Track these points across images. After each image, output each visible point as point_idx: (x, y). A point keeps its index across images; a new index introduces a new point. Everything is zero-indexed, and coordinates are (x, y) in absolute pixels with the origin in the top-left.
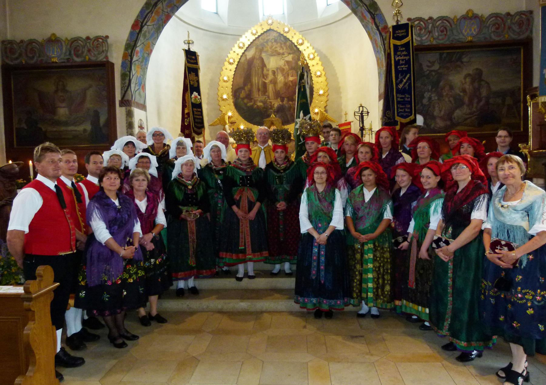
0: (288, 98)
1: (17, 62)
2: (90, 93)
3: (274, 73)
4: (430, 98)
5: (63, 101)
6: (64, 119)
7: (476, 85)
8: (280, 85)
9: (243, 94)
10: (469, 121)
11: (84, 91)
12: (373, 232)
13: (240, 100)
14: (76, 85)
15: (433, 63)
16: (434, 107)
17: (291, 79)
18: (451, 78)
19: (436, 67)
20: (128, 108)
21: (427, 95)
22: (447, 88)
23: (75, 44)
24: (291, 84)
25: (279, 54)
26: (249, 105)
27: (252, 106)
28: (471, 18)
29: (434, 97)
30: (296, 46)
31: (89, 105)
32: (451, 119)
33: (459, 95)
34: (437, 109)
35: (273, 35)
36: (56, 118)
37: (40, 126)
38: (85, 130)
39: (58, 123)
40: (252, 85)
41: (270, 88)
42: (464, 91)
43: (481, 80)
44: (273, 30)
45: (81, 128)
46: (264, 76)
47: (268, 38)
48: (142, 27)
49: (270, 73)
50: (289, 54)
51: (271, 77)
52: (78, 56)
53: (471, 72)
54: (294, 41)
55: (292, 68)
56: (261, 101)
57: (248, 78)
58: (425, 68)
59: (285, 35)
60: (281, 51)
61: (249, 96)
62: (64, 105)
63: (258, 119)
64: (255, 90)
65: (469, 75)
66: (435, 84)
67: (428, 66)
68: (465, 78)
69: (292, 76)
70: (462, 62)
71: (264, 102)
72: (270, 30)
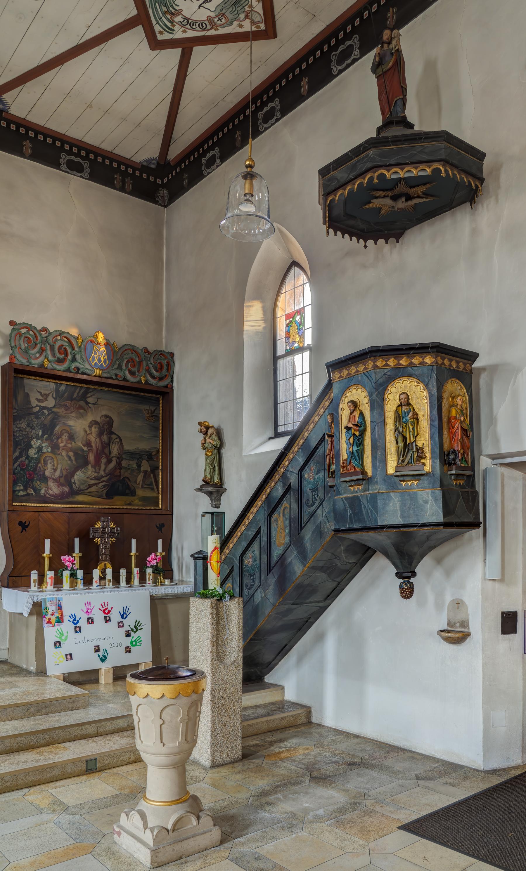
4: (40, 449)
7: (105, 438)
10: (94, 489)
15: (46, 397)
16: (46, 463)
18: (71, 423)
19: (50, 403)
21: (35, 443)
22: (65, 437)
29: (47, 448)
32: (69, 484)
33: (82, 450)
34: (49, 466)
42: (88, 444)
53: (98, 420)
58: (34, 402)
65: (96, 423)
66: (48, 430)
67: (38, 400)
68: (90, 427)
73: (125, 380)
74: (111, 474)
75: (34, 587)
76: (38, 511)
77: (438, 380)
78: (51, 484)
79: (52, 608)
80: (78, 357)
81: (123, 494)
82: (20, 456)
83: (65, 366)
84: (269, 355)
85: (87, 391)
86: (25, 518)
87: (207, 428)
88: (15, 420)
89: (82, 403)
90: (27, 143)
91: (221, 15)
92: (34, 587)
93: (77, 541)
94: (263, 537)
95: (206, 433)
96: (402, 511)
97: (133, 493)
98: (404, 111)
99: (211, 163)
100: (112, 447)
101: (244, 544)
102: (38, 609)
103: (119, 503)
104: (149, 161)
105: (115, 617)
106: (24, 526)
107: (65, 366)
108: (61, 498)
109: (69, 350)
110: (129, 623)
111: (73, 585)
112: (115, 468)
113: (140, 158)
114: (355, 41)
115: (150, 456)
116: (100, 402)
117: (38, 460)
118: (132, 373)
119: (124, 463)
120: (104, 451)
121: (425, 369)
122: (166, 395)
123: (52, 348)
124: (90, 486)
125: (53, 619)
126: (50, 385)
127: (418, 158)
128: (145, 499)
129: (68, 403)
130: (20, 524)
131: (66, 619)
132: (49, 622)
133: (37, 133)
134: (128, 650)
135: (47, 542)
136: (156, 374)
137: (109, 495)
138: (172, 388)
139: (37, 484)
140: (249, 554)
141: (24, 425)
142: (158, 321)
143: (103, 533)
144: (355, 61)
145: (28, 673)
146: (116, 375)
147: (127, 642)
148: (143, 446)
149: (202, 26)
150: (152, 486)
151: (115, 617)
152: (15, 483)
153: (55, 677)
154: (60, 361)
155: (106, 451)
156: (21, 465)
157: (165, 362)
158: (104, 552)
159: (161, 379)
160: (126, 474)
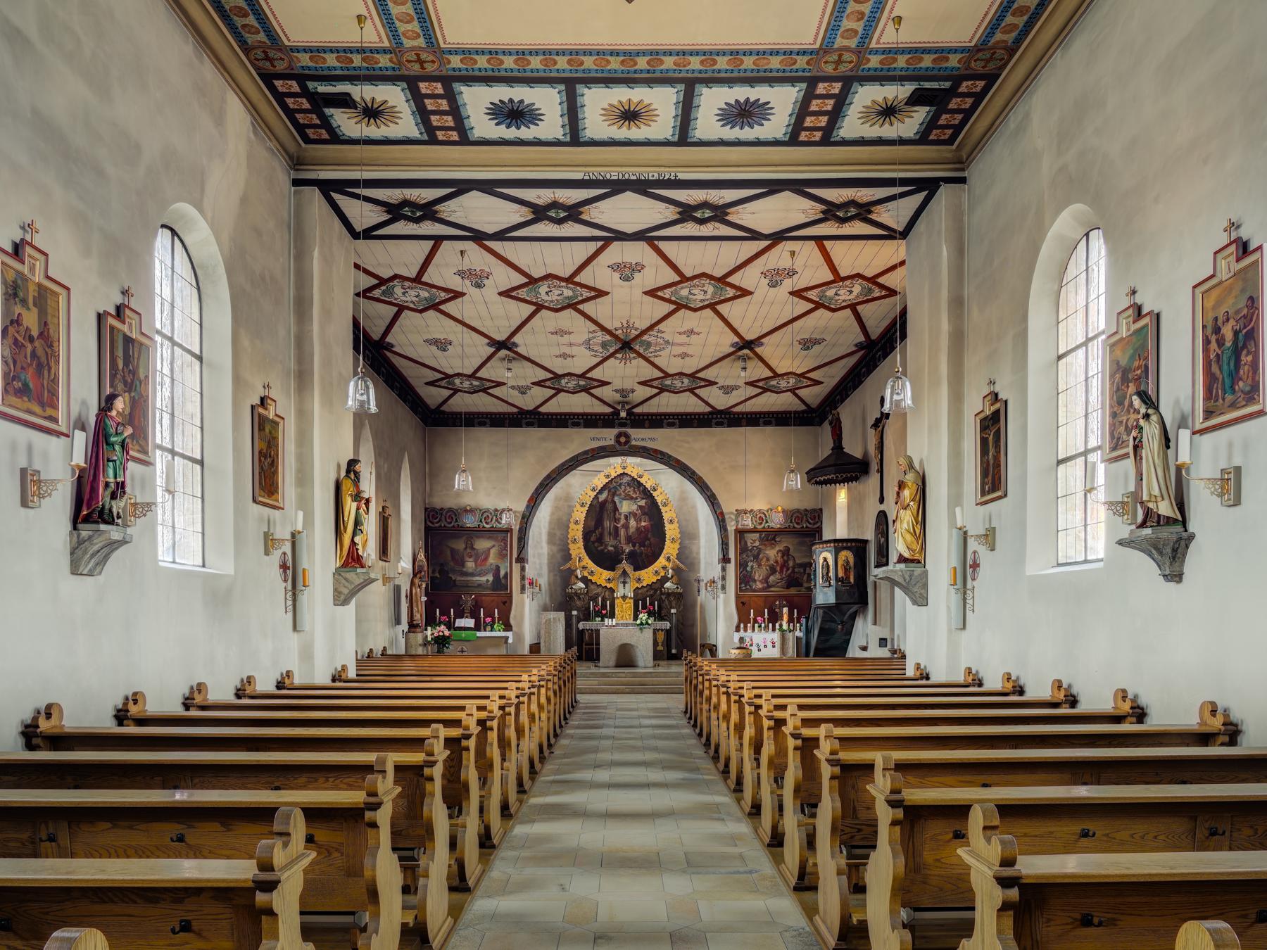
2: (492, 551)
3: (626, 517)
8: (632, 530)
11: (489, 549)
12: (797, 790)
14: (482, 544)
19: (757, 544)
23: (485, 514)
25: (632, 498)
29: (755, 566)
31: (492, 560)
35: (626, 479)
39: (466, 574)
41: (622, 532)
45: (484, 579)
46: (617, 520)
51: (623, 521)
54: (648, 486)
55: (644, 514)
57: (599, 523)
61: (600, 540)
64: (606, 533)
66: (756, 557)
71: (615, 547)
72: (624, 474)
97: (801, 585)
103: (793, 591)
106: (743, 603)
108: (763, 590)
120: (784, 565)
137: (788, 587)
153: (513, 387)
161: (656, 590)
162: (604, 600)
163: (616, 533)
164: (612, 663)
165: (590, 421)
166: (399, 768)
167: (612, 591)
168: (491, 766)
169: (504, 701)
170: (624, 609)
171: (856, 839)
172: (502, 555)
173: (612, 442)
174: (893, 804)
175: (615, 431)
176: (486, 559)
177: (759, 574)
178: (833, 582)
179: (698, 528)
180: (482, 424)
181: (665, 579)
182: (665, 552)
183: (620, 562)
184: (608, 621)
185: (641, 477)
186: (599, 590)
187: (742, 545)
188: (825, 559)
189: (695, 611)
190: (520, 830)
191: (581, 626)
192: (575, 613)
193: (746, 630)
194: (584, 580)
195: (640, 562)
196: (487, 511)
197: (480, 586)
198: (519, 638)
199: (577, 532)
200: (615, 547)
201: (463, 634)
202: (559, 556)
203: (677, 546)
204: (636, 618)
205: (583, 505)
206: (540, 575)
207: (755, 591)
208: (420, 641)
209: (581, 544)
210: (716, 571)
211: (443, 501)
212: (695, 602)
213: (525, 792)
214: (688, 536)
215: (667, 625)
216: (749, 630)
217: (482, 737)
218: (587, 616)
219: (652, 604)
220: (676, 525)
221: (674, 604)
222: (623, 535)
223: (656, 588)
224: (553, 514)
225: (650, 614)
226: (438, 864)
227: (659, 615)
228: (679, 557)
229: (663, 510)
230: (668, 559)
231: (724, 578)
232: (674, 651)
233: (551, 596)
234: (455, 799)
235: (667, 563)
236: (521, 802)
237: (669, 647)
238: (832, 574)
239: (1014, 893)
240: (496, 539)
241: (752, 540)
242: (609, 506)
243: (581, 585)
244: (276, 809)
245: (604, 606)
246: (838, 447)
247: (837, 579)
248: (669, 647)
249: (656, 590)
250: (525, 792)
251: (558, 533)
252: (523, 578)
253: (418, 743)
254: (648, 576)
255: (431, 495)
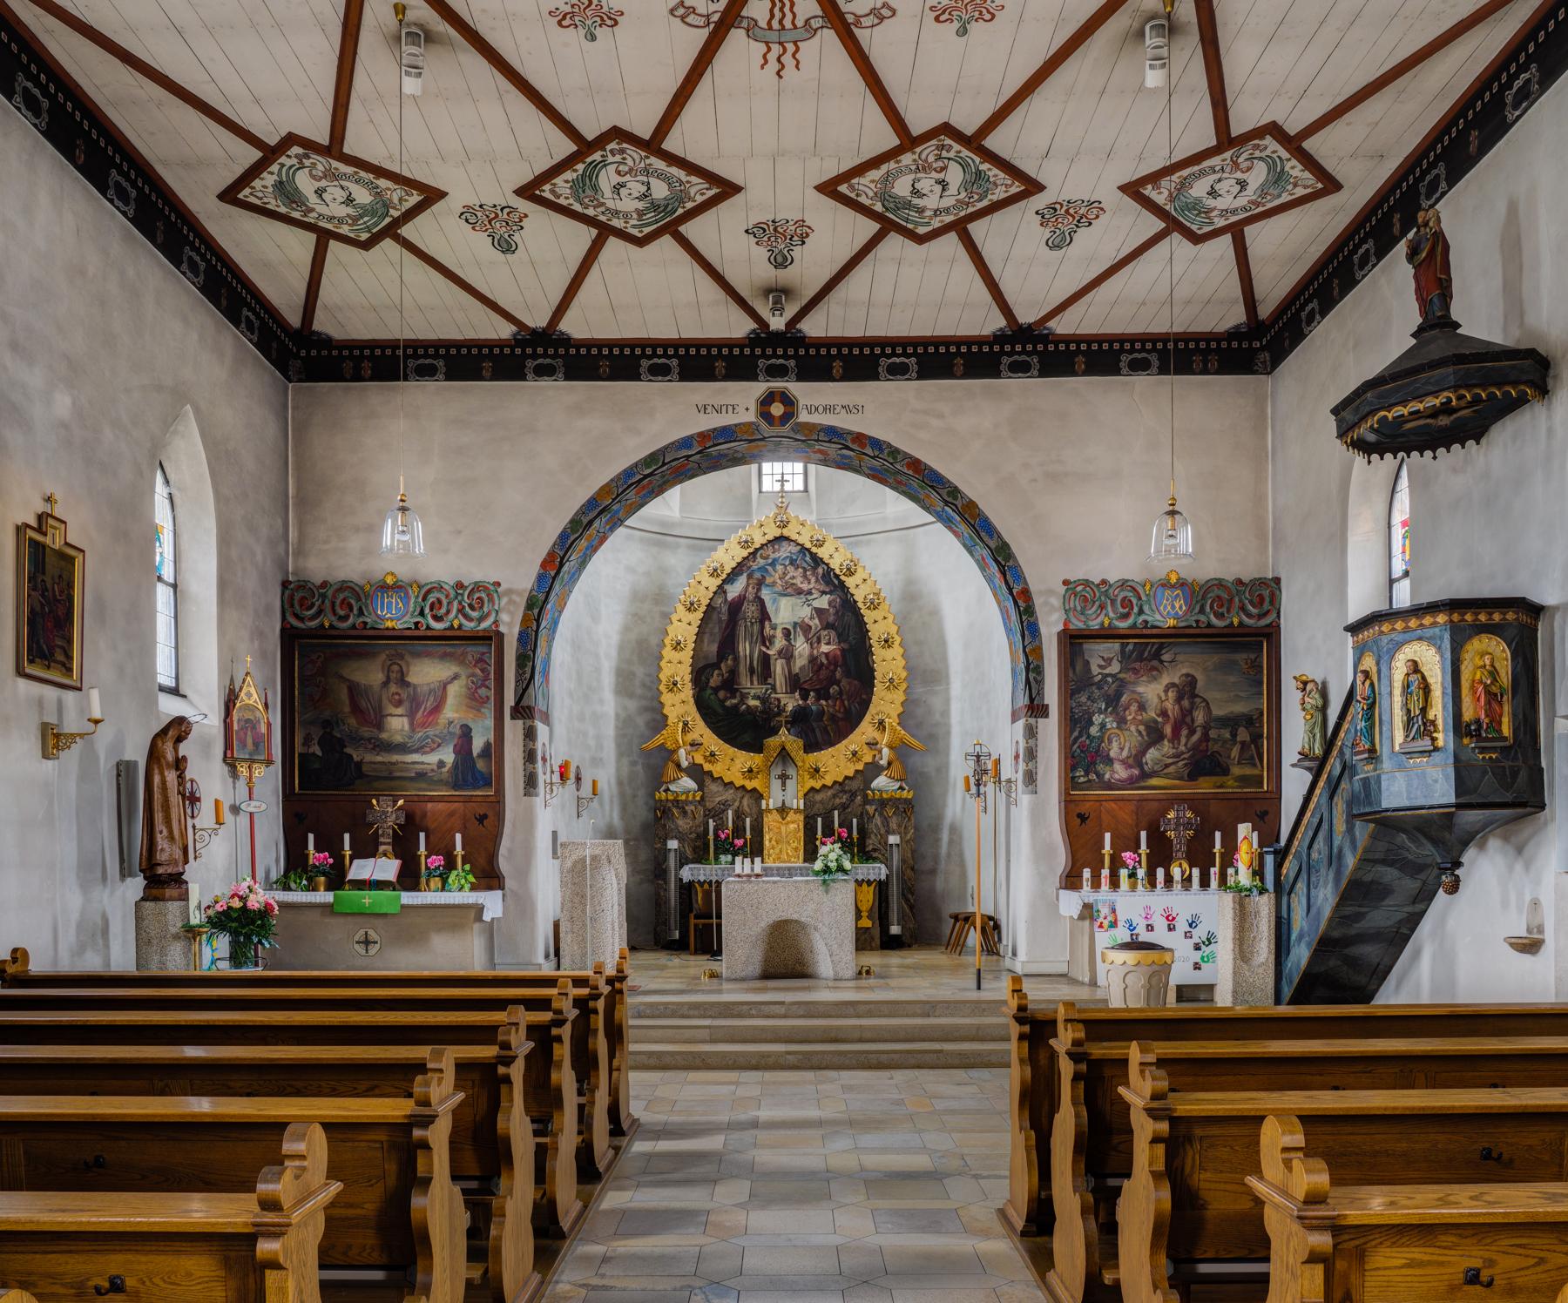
0: (817, 691)
1: (313, 624)
2: (454, 690)
4: (1103, 725)
5: (399, 704)
6: (398, 739)
7: (1186, 703)
8: (800, 662)
9: (715, 680)
10: (1171, 769)
13: (709, 691)
14: (427, 673)
15: (1109, 661)
16: (1110, 741)
17: (825, 648)
18: (1140, 689)
19: (1115, 668)
20: (529, 722)
21: (1097, 719)
22: (1134, 708)
23: (430, 596)
24: (824, 661)
25: (799, 592)
26: (728, 703)
27: (736, 707)
28: (1173, 587)
29: (1111, 723)
30: (837, 576)
31: (453, 711)
32: (1140, 765)
33: (1156, 722)
34: (1115, 745)
36: (384, 736)
37: (348, 750)
38: (441, 764)
40: (736, 659)
41: (779, 667)
42: (1164, 713)
43: (1193, 696)
44: (787, 539)
45: (432, 759)
46: (766, 641)
47: (777, 555)
48: (561, 565)
49: (779, 633)
50: (823, 593)
51: (780, 643)
52: (437, 618)
53: (1176, 681)
54: (835, 564)
55: (827, 626)
56: (756, 697)
57: (728, 645)
58: (1095, 670)
59: (814, 550)
60: (805, 587)
61: (730, 684)
62: (399, 711)
63: (747, 738)
64: (743, 670)
65: (1173, 685)
66: (1113, 701)
67: (1100, 667)
68: (1166, 691)
69: (828, 644)
70: (1162, 662)
71: (764, 700)
73: (1209, 625)
74: (1195, 748)
75: (1086, 887)
76: (1100, 801)
77: (1453, 641)
78: (1117, 766)
79: (1105, 911)
80: (1146, 608)
81: (1211, 773)
82: (1080, 735)
83: (1130, 621)
84: (1383, 580)
85: (1161, 646)
86: (1084, 808)
87: (1305, 683)
88: (1072, 695)
89: (1155, 663)
90: (1081, 358)
91: (1263, 194)
92: (1086, 887)
93: (1143, 834)
94: (1325, 826)
95: (1304, 690)
96: (1409, 792)
97: (1225, 771)
98: (1446, 307)
99: (1310, 319)
100: (1195, 714)
101: (1311, 833)
102: (1088, 911)
103: (1205, 786)
104: (1237, 327)
105: (1182, 926)
106: (1083, 818)
107: (1130, 621)
108: (1131, 783)
109: (1134, 601)
110: (1200, 934)
111: (1133, 887)
112: (1200, 741)
113: (1224, 326)
114: (1441, 169)
115: (1251, 721)
116: (1180, 658)
117: (1101, 739)
118: (1220, 616)
119: (1213, 734)
120: (1183, 722)
121: (1437, 630)
122: (1271, 635)
123: (1113, 602)
124: (1167, 766)
125: (1106, 923)
126: (1115, 646)
127: (1421, 392)
128: (1244, 780)
129: (1137, 665)
130: (1079, 815)
131: (1120, 924)
132: (1101, 926)
133: (1089, 343)
134: (1197, 967)
135: (1108, 836)
136: (1254, 611)
137: (1192, 777)
138: (1279, 627)
139: (1100, 767)
140: (1315, 846)
141: (1083, 699)
142: (1261, 535)
143: (1178, 824)
144: (1444, 194)
145: (1083, 984)
146: (1197, 622)
147: (1197, 957)
148: (1240, 708)
149: (1244, 209)
150: (1253, 759)
151: (1182, 926)
152: (1074, 768)
154: (1125, 616)
155: (1188, 719)
156: (1082, 746)
157: (1266, 592)
158: (1179, 848)
159: (1260, 617)
160: (1216, 748)
161: (853, 794)
162: (739, 816)
163: (764, 669)
164: (755, 967)
165: (696, 361)
166: (462, 1067)
167: (757, 795)
168: (556, 1100)
169: (586, 991)
170: (783, 836)
171: (1103, 1155)
172: (474, 700)
173: (751, 417)
174: (1153, 1114)
175: (759, 388)
176: (437, 709)
177: (1120, 746)
178: (1444, 738)
179: (944, 659)
180: (426, 372)
181: (873, 769)
182: (872, 709)
183: (774, 732)
184: (742, 865)
185: (820, 544)
186: (729, 795)
187: (1086, 658)
188: (1415, 667)
189: (938, 840)
190: (612, 1199)
191: (687, 873)
192: (673, 844)
193: (1096, 885)
194: (696, 772)
195: (821, 730)
196: (439, 587)
197: (421, 776)
198: (522, 906)
199: (678, 666)
200: (764, 700)
201: (367, 898)
202: (641, 721)
203: (899, 696)
204: (811, 854)
205: (691, 608)
206: (596, 762)
207: (1109, 786)
208: (175, 926)
209: (688, 692)
210: (1006, 739)
211: (336, 560)
212: (939, 818)
213: (622, 1133)
214: (926, 675)
215: (878, 871)
216: (1105, 887)
217: (541, 1061)
218: (700, 856)
219: (845, 823)
220: (897, 651)
221: (893, 825)
222: (785, 678)
223: (854, 789)
224: (626, 629)
225: (847, 846)
226: (517, 1198)
227: (860, 849)
228: (903, 719)
229: (869, 616)
230: (881, 725)
231: (1031, 754)
232: (895, 930)
233: (624, 808)
234: (585, 1065)
235: (877, 735)
236: (617, 1149)
237: (884, 921)
238: (1439, 710)
239: (1083, 1067)
240: (460, 660)
241: (1102, 659)
242: (750, 610)
243: (687, 783)
244: (287, 1124)
245: (739, 831)
246: (1437, 318)
247: (1460, 728)
248: (884, 921)
249: (853, 794)
250: (622, 1133)
251: (640, 671)
252: (530, 756)
253: (485, 1034)
254: (836, 762)
255: (300, 552)
